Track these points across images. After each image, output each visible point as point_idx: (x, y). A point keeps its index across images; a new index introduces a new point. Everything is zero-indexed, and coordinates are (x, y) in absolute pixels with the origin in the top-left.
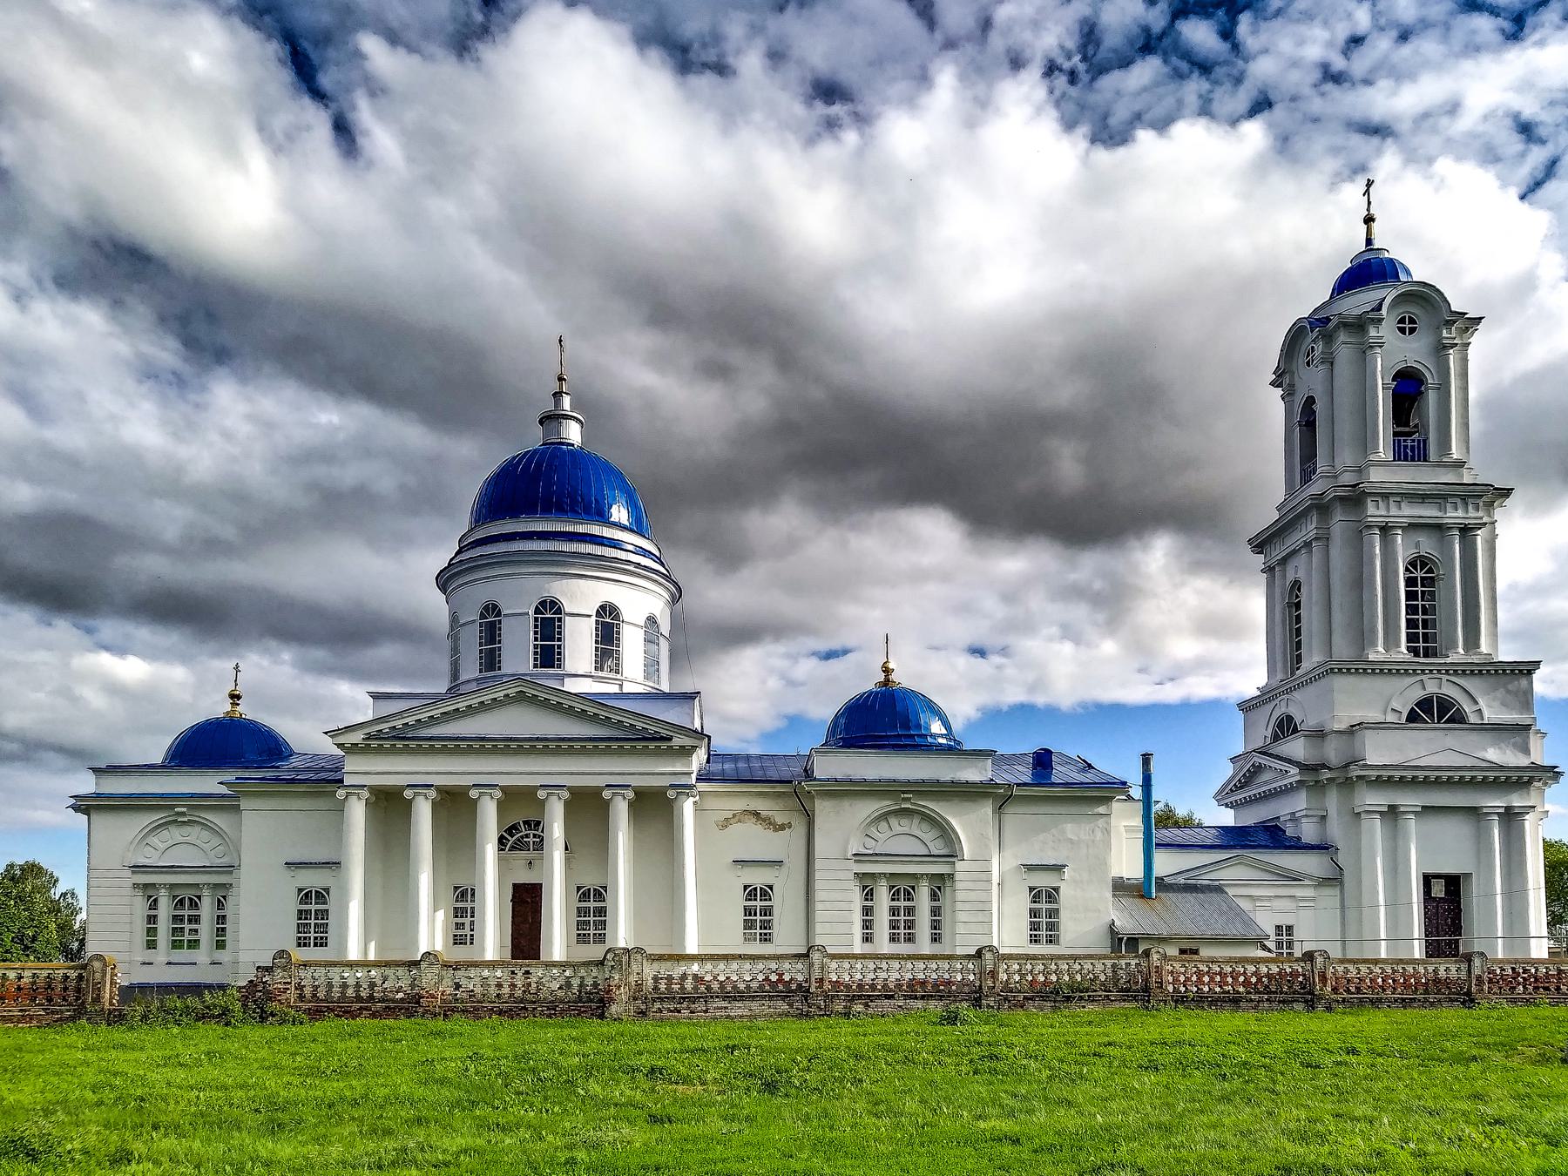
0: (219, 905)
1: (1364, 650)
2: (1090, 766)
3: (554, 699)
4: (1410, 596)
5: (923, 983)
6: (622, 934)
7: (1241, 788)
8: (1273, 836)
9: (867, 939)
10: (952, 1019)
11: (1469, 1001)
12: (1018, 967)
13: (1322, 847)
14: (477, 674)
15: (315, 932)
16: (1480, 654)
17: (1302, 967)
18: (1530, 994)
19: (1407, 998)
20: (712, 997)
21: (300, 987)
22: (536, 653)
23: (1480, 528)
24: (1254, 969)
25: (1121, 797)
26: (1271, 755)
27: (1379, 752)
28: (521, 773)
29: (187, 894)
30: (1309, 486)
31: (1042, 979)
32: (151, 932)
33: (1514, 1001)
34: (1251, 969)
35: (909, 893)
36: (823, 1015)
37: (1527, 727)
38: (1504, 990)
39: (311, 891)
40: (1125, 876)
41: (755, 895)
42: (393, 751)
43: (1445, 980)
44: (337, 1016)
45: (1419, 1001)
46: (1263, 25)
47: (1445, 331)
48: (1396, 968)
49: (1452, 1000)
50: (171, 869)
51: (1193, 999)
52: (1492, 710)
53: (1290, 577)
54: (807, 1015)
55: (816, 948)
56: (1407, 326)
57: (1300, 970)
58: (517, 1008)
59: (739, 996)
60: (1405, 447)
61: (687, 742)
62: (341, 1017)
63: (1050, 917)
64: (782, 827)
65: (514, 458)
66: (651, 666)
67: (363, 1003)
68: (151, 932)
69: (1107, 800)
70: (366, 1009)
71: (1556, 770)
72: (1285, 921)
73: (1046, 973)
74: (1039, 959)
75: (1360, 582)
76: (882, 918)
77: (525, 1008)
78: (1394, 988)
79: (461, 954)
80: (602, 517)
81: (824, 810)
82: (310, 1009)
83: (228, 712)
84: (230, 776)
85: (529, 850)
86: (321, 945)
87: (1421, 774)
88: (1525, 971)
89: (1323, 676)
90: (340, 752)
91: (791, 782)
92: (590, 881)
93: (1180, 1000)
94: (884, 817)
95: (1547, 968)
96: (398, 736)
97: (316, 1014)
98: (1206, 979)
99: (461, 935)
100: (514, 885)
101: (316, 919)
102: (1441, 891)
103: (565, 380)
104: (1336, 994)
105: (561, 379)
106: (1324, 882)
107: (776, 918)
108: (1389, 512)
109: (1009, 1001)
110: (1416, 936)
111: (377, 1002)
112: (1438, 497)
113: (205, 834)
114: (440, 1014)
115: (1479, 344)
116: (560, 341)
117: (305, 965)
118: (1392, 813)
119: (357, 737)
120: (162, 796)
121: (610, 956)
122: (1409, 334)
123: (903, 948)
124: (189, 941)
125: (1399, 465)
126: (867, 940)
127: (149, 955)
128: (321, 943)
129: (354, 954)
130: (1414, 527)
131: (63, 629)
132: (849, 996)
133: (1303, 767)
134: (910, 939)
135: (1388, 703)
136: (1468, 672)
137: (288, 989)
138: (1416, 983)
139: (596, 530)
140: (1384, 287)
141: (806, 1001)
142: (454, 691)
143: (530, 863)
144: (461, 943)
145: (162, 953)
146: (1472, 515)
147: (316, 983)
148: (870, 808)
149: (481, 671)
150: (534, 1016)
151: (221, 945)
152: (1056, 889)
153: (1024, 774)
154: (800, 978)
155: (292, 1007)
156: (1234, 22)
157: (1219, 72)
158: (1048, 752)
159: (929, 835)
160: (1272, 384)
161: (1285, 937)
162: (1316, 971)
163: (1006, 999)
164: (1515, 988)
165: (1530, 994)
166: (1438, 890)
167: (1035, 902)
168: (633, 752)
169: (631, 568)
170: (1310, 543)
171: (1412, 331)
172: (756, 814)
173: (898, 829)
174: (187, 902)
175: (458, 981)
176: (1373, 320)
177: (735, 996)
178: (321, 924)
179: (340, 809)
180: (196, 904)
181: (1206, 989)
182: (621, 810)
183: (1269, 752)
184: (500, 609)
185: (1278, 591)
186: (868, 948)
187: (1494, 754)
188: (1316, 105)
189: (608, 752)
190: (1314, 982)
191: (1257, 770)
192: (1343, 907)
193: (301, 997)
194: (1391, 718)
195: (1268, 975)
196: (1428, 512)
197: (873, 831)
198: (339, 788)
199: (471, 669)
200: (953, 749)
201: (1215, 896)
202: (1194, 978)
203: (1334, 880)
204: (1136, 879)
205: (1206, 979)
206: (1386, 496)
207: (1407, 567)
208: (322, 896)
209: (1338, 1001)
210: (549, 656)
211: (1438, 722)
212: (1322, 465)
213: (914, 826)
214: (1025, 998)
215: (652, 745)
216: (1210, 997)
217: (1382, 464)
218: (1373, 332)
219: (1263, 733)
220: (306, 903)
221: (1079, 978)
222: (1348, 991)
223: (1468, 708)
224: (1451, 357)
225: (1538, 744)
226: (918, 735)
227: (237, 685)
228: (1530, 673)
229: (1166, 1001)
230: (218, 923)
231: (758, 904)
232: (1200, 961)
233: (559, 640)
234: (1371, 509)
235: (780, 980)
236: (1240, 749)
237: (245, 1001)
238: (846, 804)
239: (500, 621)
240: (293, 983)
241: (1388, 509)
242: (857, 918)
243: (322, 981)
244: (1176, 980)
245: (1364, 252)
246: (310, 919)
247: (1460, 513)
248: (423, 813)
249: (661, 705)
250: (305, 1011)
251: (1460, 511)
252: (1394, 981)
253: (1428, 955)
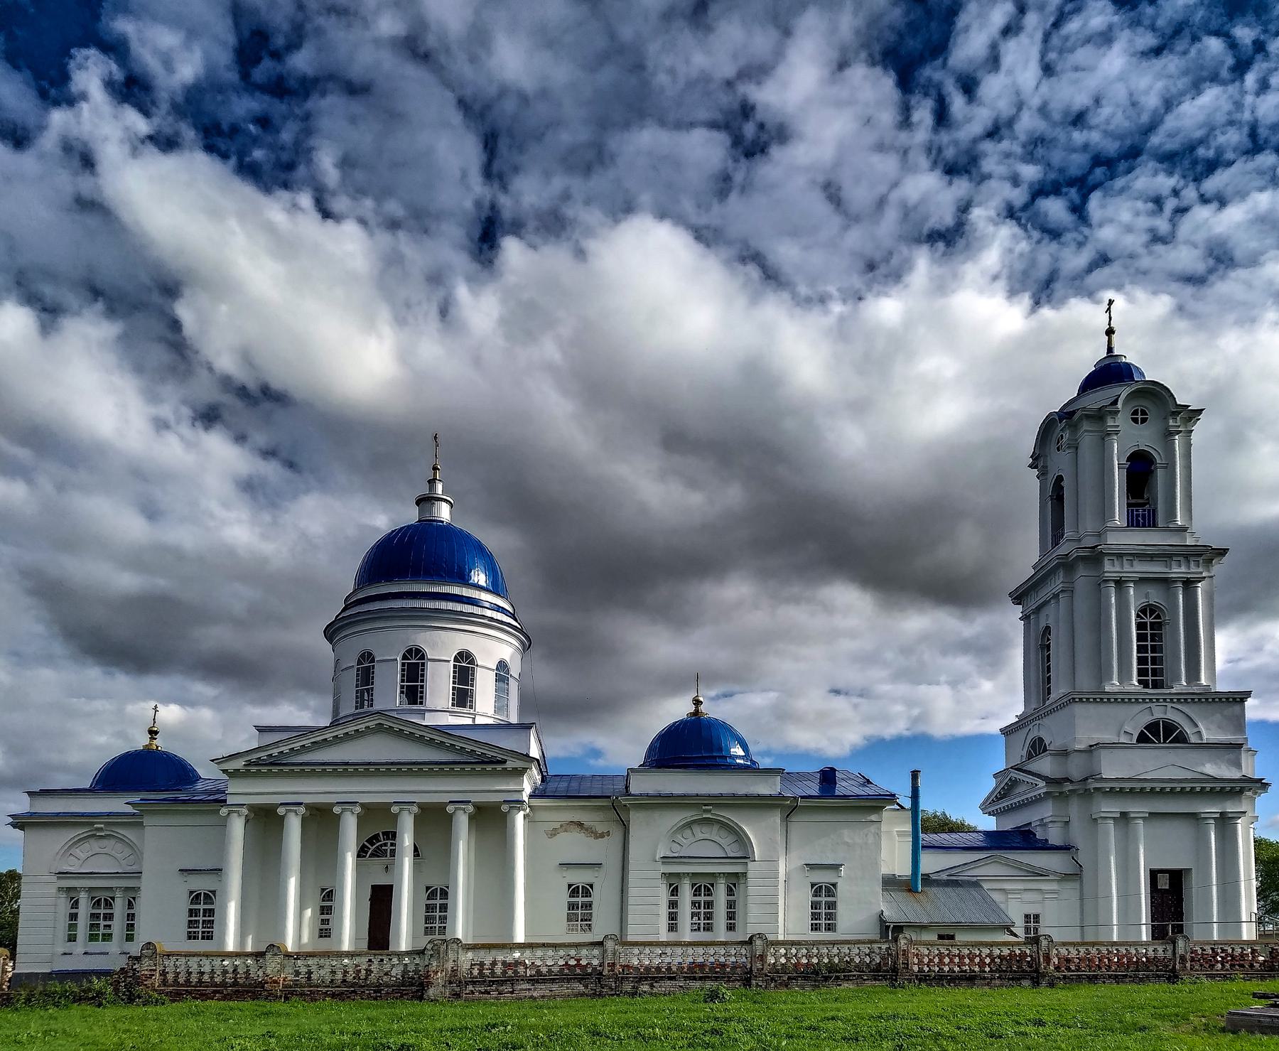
0: (129, 905)
1: (1102, 683)
2: (869, 782)
3: (407, 730)
4: (1141, 638)
5: (702, 966)
6: (460, 927)
7: (1001, 798)
8: (1024, 839)
9: (672, 928)
10: (713, 996)
11: (1173, 977)
12: (785, 951)
13: (1066, 848)
14: (353, 711)
15: (203, 928)
16: (1201, 685)
17: (1030, 949)
18: (1227, 970)
19: (1119, 975)
20: (518, 980)
21: (164, 973)
23: (1200, 582)
24: (989, 951)
25: (892, 807)
26: (1025, 771)
27: (1113, 768)
28: (386, 792)
29: (103, 895)
30: (1058, 548)
31: (804, 961)
32: (72, 927)
33: (1212, 977)
34: (986, 951)
35: (709, 890)
36: (613, 995)
37: (1240, 746)
38: (1205, 967)
39: (201, 893)
40: (897, 873)
41: (578, 893)
42: (269, 775)
43: (1154, 959)
44: (194, 998)
45: (1131, 977)
46: (1108, 200)
47: (1171, 421)
48: (1111, 950)
49: (1159, 976)
50: (91, 875)
51: (934, 978)
52: (1209, 734)
53: (1043, 625)
54: (600, 995)
55: (609, 937)
56: (1139, 417)
57: (1028, 952)
58: (377, 992)
59: (541, 979)
60: (1138, 516)
61: (519, 764)
62: (197, 999)
63: (829, 909)
64: (602, 836)
65: (393, 531)
66: (501, 705)
67: (217, 987)
68: (72, 927)
69: (878, 809)
70: (218, 992)
71: (1263, 781)
72: (1032, 910)
73: (809, 957)
74: (803, 945)
75: (1099, 625)
76: (685, 909)
77: (354, 992)
78: (1109, 966)
79: (324, 945)
80: (464, 580)
81: (637, 820)
82: (171, 992)
83: (147, 745)
84: (136, 798)
85: (386, 856)
86: (208, 939)
87: (1148, 786)
88: (1223, 951)
89: (1067, 705)
90: (225, 777)
91: (609, 797)
92: (437, 883)
93: (923, 978)
94: (689, 825)
95: (1241, 948)
96: (273, 762)
97: (176, 996)
98: (977, 960)
99: (326, 930)
100: (373, 887)
101: (204, 916)
102: (1166, 884)
103: (439, 469)
104: (1059, 972)
105: (435, 469)
106: (1066, 877)
107: (595, 910)
108: (1123, 568)
109: (776, 981)
110: (1144, 922)
111: (229, 987)
112: (1165, 556)
113: (119, 845)
114: (281, 997)
115: (1200, 431)
116: (435, 438)
117: (168, 956)
118: (1124, 818)
119: (239, 764)
120: (83, 815)
121: (429, 947)
122: (1141, 424)
123: (703, 936)
124: (104, 935)
125: (1132, 531)
126: (731, 929)
128: (208, 936)
129: (231, 946)
130: (1142, 581)
131: (122, 681)
132: (637, 977)
133: (1049, 781)
134: (708, 928)
135: (1122, 726)
136: (1196, 700)
137: (153, 975)
138: (1128, 962)
139: (456, 590)
140: (1121, 386)
141: (599, 982)
142: (335, 723)
143: (387, 867)
144: (326, 936)
146: (1194, 570)
147: (178, 970)
148: (675, 818)
149: (356, 708)
150: (362, 999)
151: (130, 938)
152: (834, 885)
153: (813, 788)
154: (595, 962)
155: (156, 990)
156: (1085, 198)
157: (1068, 237)
158: (833, 770)
159: (725, 840)
160: (1030, 466)
161: (1032, 924)
162: (1041, 953)
163: (772, 979)
164: (1213, 965)
165: (1227, 970)
166: (1164, 883)
167: (816, 896)
168: (473, 773)
169: (389, 614)
170: (1057, 595)
171: (1144, 421)
172: (580, 825)
173: (701, 836)
174: (102, 902)
175: (297, 969)
176: (1110, 412)
177: (538, 979)
178: (209, 921)
179: (223, 824)
180: (111, 905)
181: (946, 969)
182: (462, 823)
183: (1024, 768)
184: (373, 657)
185: (1032, 634)
186: (672, 937)
187: (1211, 769)
188: (1145, 262)
189: (452, 773)
190: (1039, 962)
191: (1014, 783)
192: (1082, 899)
193: (164, 982)
194: (1123, 739)
195: (1000, 956)
196: (1156, 569)
197: (679, 838)
198: (222, 806)
199: (348, 708)
200: (751, 769)
201: (973, 892)
202: (936, 960)
203: (1075, 875)
204: (906, 876)
205: (947, 960)
206: (1120, 556)
207: (1138, 614)
208: (209, 897)
209: (1059, 978)
210: (414, 694)
211: (1164, 742)
212: (1068, 533)
213: (713, 833)
214: (789, 978)
215: (489, 768)
216: (949, 976)
217: (1118, 529)
218: (1110, 422)
219: (1020, 753)
220: (196, 904)
221: (836, 960)
222: (1069, 969)
223: (1189, 730)
224: (1177, 442)
225: (1249, 761)
226: (720, 757)
227: (155, 722)
228: (1242, 701)
229: (911, 979)
230: (128, 920)
231: (580, 900)
232: (941, 945)
233: (422, 681)
234: (1108, 566)
235: (578, 965)
236: (1002, 767)
237: (117, 985)
238: (656, 814)
239: (373, 666)
240: (158, 970)
241: (1122, 566)
242: (664, 911)
243: (207, 969)
244: (920, 962)
245: (1105, 358)
246: (436, 912)
247: (1183, 569)
248: (294, 827)
249: (503, 733)
250: (167, 993)
251: (1183, 567)
252: (1109, 960)
253: (1154, 938)
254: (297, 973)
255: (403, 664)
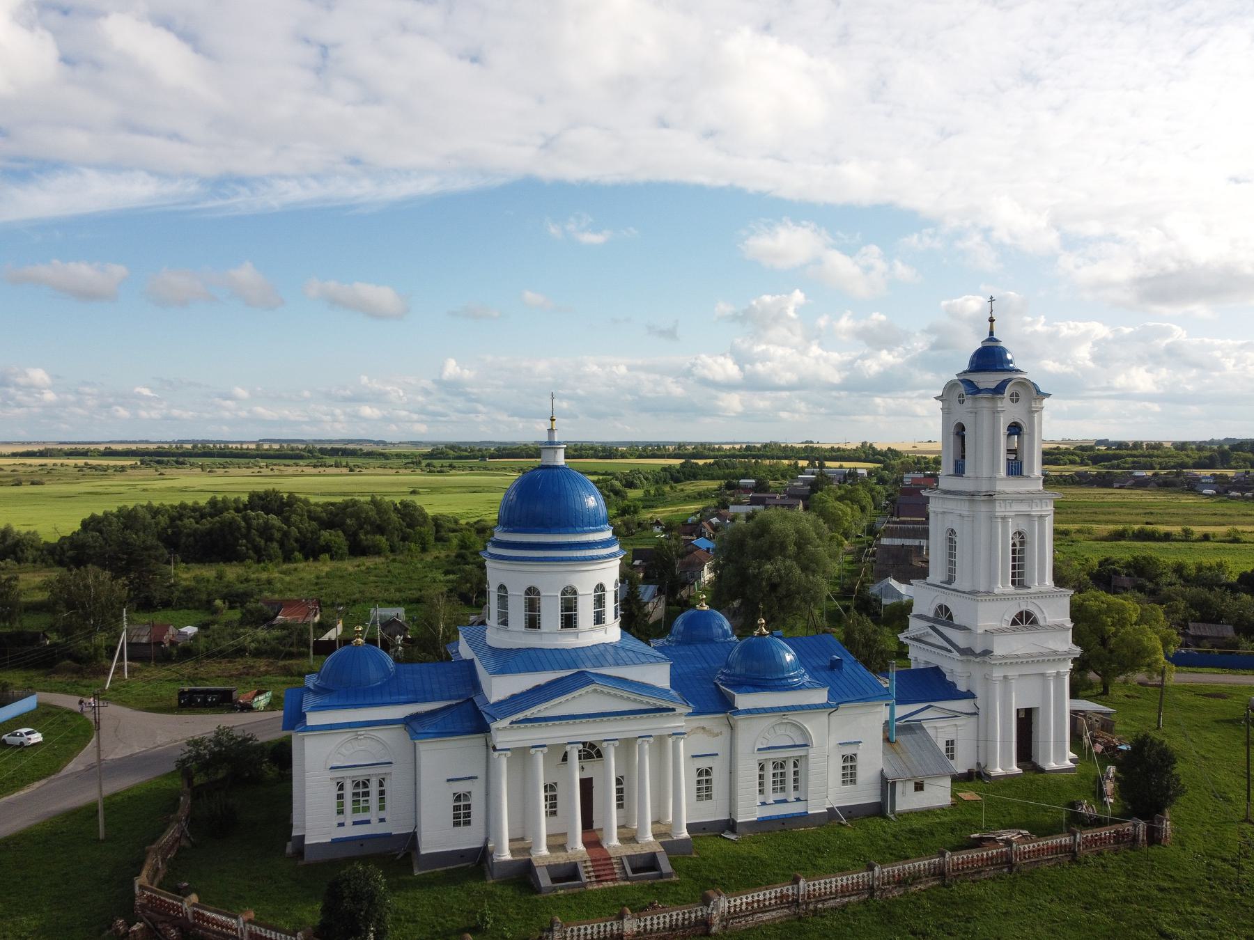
22: (562, 619)
32: (341, 805)
68: (341, 805)
76: (769, 779)
123: (780, 796)
127: (341, 819)
134: (783, 789)
145: (349, 817)
151: (382, 808)
166: (1022, 715)
172: (703, 728)
194: (1004, 625)
196: (1024, 508)
217: (1002, 479)
254: (639, 927)
255: (562, 599)
